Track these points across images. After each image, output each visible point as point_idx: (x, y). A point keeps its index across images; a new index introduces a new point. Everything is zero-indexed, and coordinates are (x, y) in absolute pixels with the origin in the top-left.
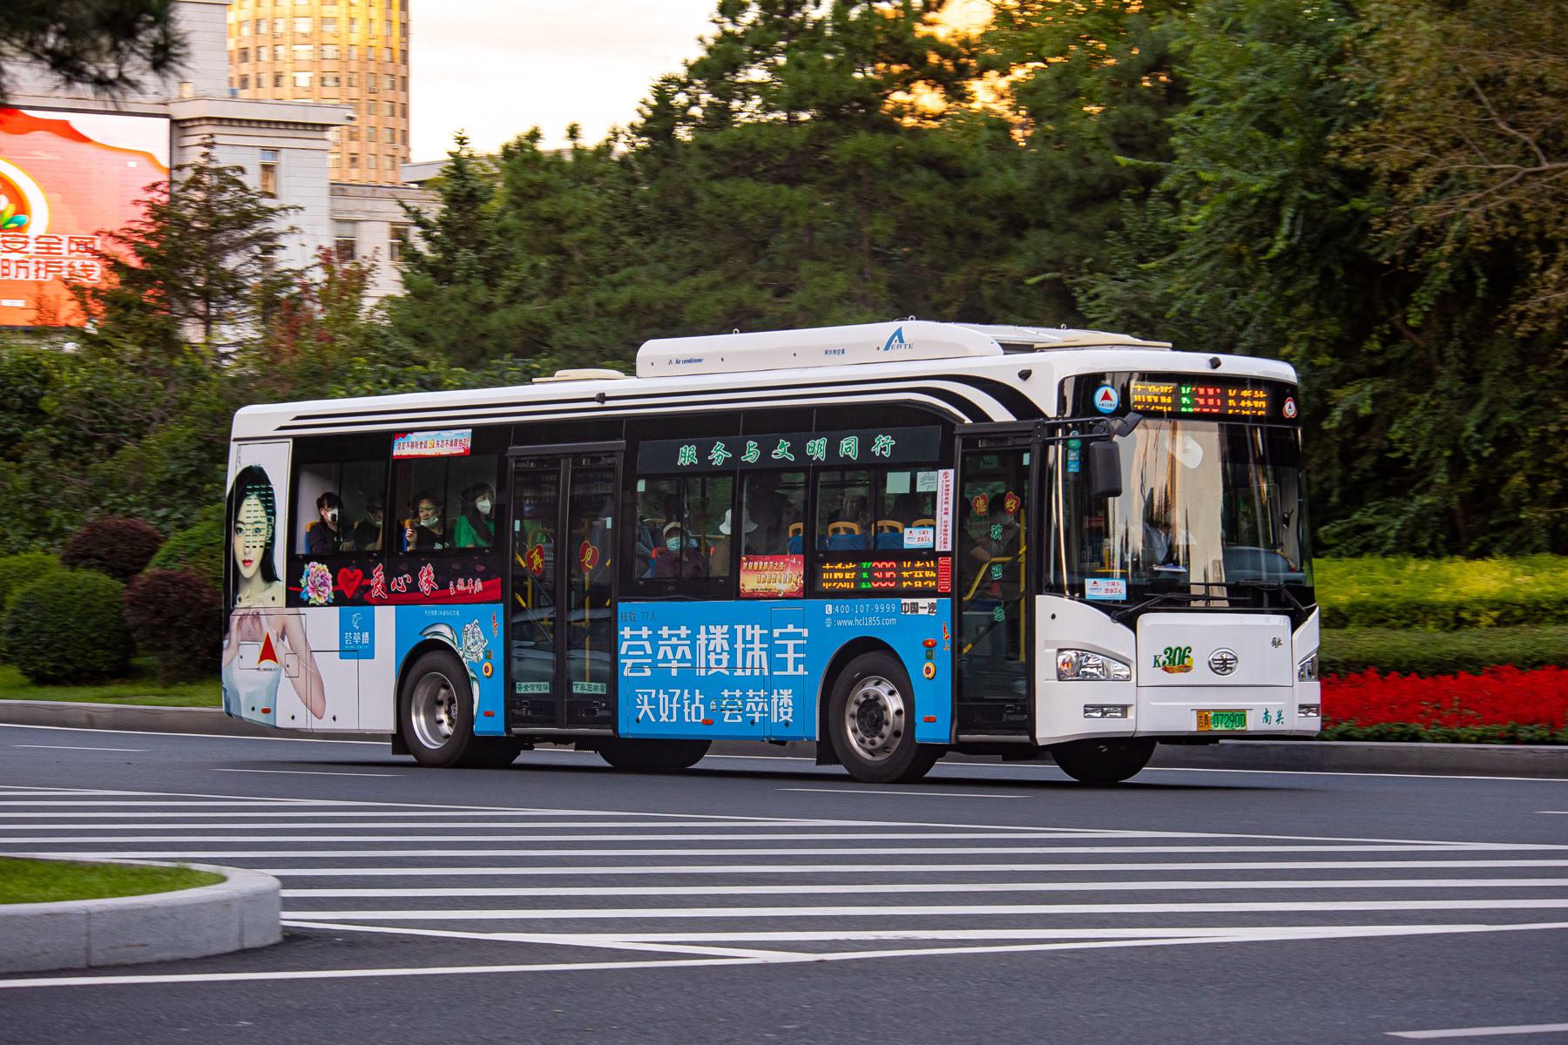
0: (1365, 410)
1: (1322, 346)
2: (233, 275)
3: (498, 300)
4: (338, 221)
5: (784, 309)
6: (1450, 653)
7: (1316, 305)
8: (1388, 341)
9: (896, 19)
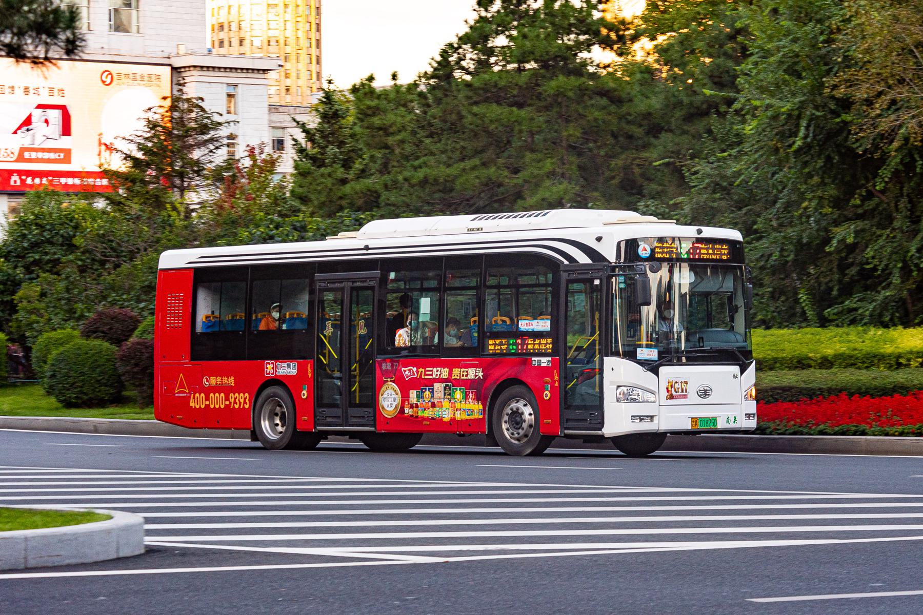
0: (850, 240)
1: (826, 202)
2: (197, 162)
3: (351, 177)
4: (274, 127)
5: (516, 181)
6: (890, 383)
7: (822, 178)
8: (864, 199)
9: (582, 8)
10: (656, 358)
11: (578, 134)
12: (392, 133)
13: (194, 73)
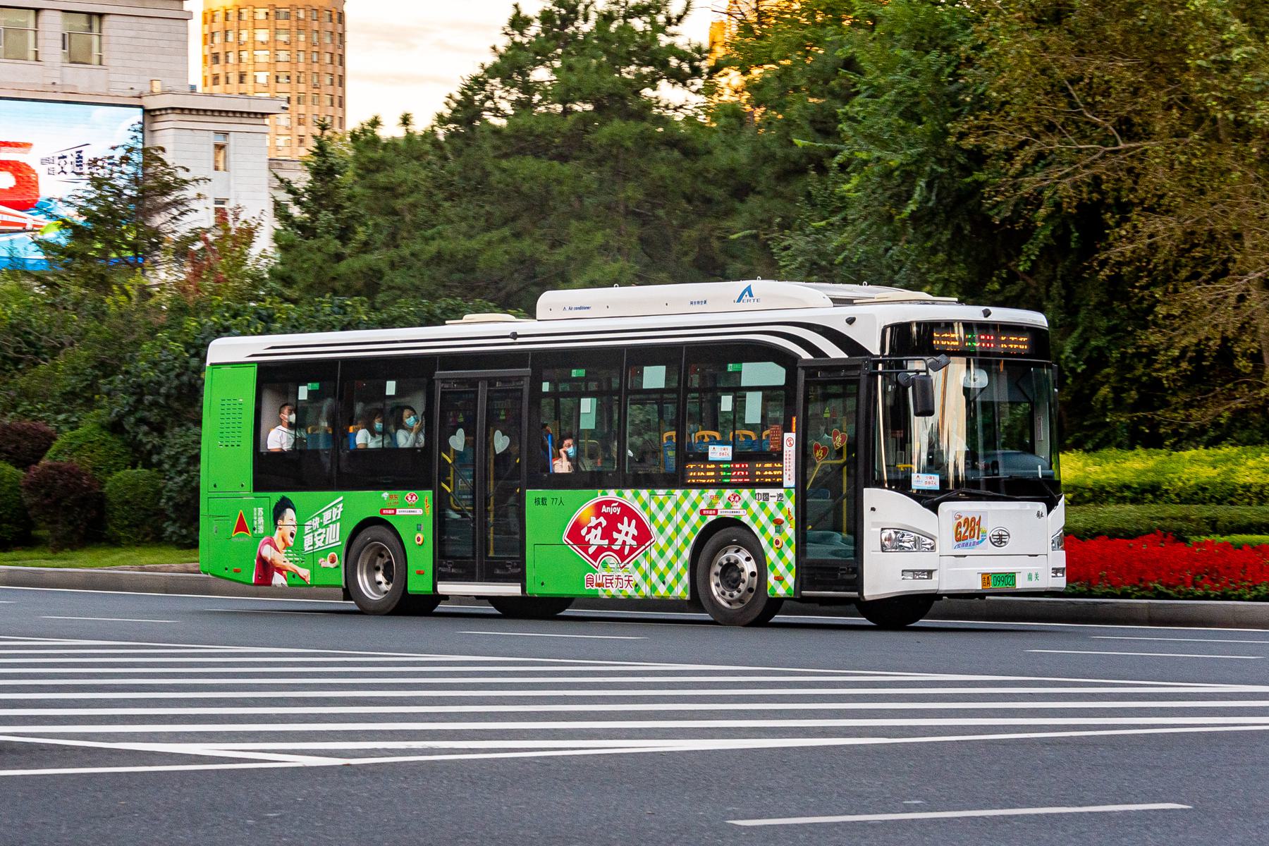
3: (347, 251)
5: (557, 257)
7: (949, 255)
9: (645, 31)
10: (937, 487)
11: (640, 197)
12: (402, 195)
13: (172, 117)
